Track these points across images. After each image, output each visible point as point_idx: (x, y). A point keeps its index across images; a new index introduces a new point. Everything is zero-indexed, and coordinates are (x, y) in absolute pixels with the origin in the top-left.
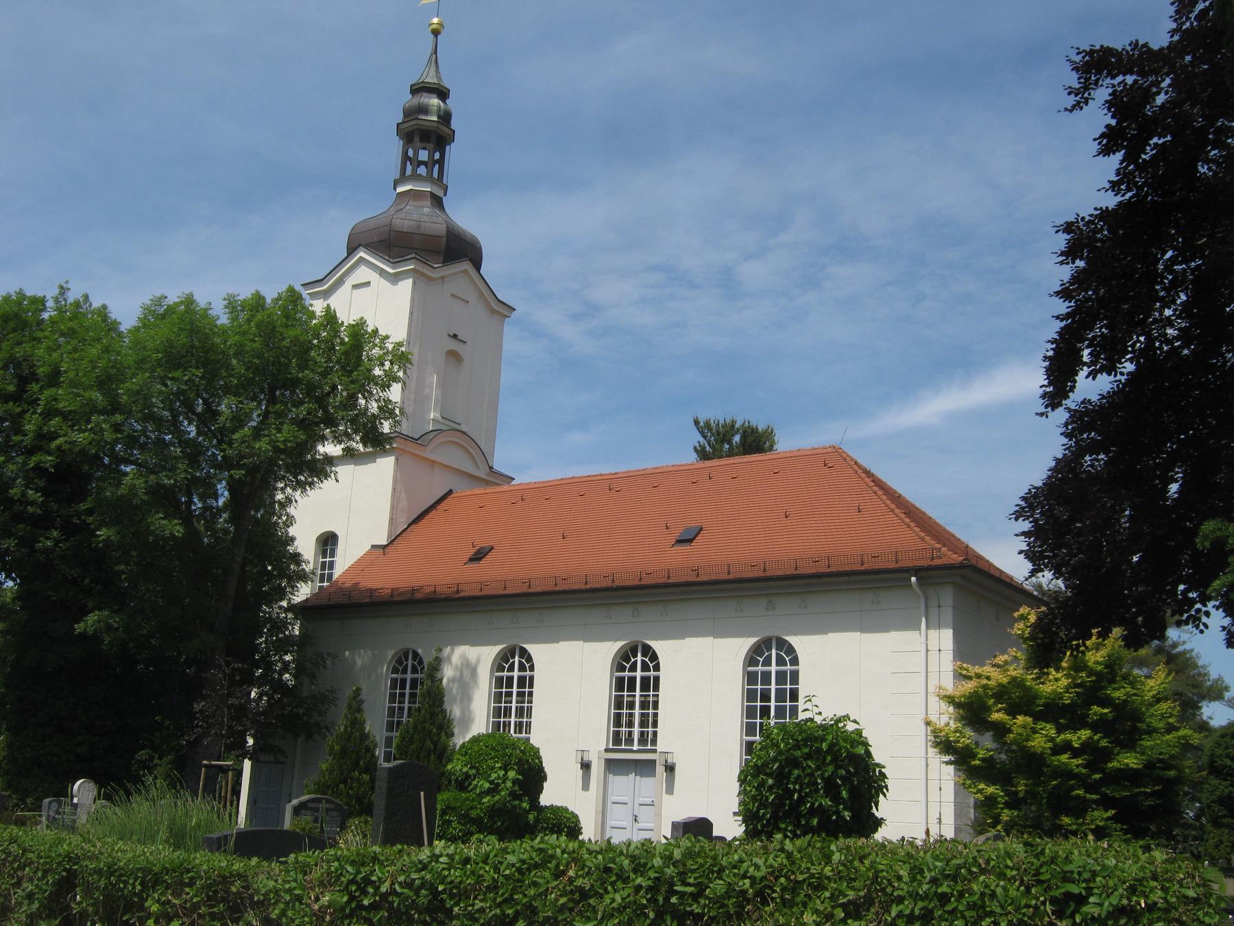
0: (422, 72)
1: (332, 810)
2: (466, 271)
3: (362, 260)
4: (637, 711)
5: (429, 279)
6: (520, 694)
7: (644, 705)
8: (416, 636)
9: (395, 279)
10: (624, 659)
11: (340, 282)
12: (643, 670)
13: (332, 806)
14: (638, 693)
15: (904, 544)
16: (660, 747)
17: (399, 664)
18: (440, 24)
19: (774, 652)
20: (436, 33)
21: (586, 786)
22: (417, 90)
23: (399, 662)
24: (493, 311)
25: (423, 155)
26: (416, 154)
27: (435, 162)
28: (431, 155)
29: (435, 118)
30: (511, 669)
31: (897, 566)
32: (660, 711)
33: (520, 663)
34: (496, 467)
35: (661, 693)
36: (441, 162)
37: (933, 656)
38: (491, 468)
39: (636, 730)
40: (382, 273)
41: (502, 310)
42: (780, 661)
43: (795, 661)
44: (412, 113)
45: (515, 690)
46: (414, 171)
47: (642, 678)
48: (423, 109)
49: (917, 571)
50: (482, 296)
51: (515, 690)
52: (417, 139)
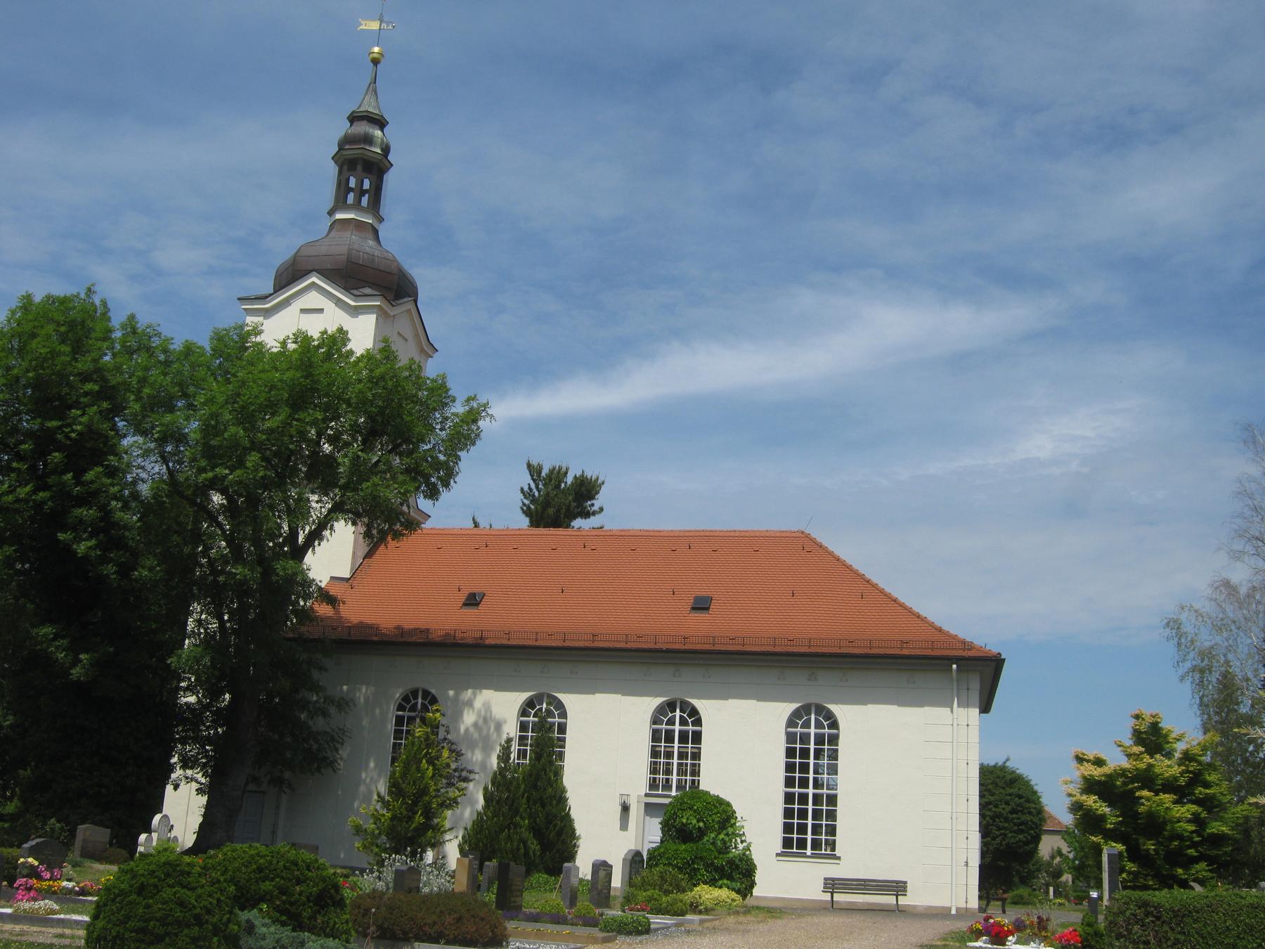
3: (314, 284)
4: (675, 761)
8: (425, 675)
9: (355, 312)
11: (286, 303)
12: (681, 724)
14: (676, 744)
17: (407, 701)
19: (813, 717)
21: (624, 825)
22: (353, 118)
40: (338, 302)
43: (698, 722)
44: (346, 141)
48: (368, 140)
49: (957, 660)
52: (359, 168)
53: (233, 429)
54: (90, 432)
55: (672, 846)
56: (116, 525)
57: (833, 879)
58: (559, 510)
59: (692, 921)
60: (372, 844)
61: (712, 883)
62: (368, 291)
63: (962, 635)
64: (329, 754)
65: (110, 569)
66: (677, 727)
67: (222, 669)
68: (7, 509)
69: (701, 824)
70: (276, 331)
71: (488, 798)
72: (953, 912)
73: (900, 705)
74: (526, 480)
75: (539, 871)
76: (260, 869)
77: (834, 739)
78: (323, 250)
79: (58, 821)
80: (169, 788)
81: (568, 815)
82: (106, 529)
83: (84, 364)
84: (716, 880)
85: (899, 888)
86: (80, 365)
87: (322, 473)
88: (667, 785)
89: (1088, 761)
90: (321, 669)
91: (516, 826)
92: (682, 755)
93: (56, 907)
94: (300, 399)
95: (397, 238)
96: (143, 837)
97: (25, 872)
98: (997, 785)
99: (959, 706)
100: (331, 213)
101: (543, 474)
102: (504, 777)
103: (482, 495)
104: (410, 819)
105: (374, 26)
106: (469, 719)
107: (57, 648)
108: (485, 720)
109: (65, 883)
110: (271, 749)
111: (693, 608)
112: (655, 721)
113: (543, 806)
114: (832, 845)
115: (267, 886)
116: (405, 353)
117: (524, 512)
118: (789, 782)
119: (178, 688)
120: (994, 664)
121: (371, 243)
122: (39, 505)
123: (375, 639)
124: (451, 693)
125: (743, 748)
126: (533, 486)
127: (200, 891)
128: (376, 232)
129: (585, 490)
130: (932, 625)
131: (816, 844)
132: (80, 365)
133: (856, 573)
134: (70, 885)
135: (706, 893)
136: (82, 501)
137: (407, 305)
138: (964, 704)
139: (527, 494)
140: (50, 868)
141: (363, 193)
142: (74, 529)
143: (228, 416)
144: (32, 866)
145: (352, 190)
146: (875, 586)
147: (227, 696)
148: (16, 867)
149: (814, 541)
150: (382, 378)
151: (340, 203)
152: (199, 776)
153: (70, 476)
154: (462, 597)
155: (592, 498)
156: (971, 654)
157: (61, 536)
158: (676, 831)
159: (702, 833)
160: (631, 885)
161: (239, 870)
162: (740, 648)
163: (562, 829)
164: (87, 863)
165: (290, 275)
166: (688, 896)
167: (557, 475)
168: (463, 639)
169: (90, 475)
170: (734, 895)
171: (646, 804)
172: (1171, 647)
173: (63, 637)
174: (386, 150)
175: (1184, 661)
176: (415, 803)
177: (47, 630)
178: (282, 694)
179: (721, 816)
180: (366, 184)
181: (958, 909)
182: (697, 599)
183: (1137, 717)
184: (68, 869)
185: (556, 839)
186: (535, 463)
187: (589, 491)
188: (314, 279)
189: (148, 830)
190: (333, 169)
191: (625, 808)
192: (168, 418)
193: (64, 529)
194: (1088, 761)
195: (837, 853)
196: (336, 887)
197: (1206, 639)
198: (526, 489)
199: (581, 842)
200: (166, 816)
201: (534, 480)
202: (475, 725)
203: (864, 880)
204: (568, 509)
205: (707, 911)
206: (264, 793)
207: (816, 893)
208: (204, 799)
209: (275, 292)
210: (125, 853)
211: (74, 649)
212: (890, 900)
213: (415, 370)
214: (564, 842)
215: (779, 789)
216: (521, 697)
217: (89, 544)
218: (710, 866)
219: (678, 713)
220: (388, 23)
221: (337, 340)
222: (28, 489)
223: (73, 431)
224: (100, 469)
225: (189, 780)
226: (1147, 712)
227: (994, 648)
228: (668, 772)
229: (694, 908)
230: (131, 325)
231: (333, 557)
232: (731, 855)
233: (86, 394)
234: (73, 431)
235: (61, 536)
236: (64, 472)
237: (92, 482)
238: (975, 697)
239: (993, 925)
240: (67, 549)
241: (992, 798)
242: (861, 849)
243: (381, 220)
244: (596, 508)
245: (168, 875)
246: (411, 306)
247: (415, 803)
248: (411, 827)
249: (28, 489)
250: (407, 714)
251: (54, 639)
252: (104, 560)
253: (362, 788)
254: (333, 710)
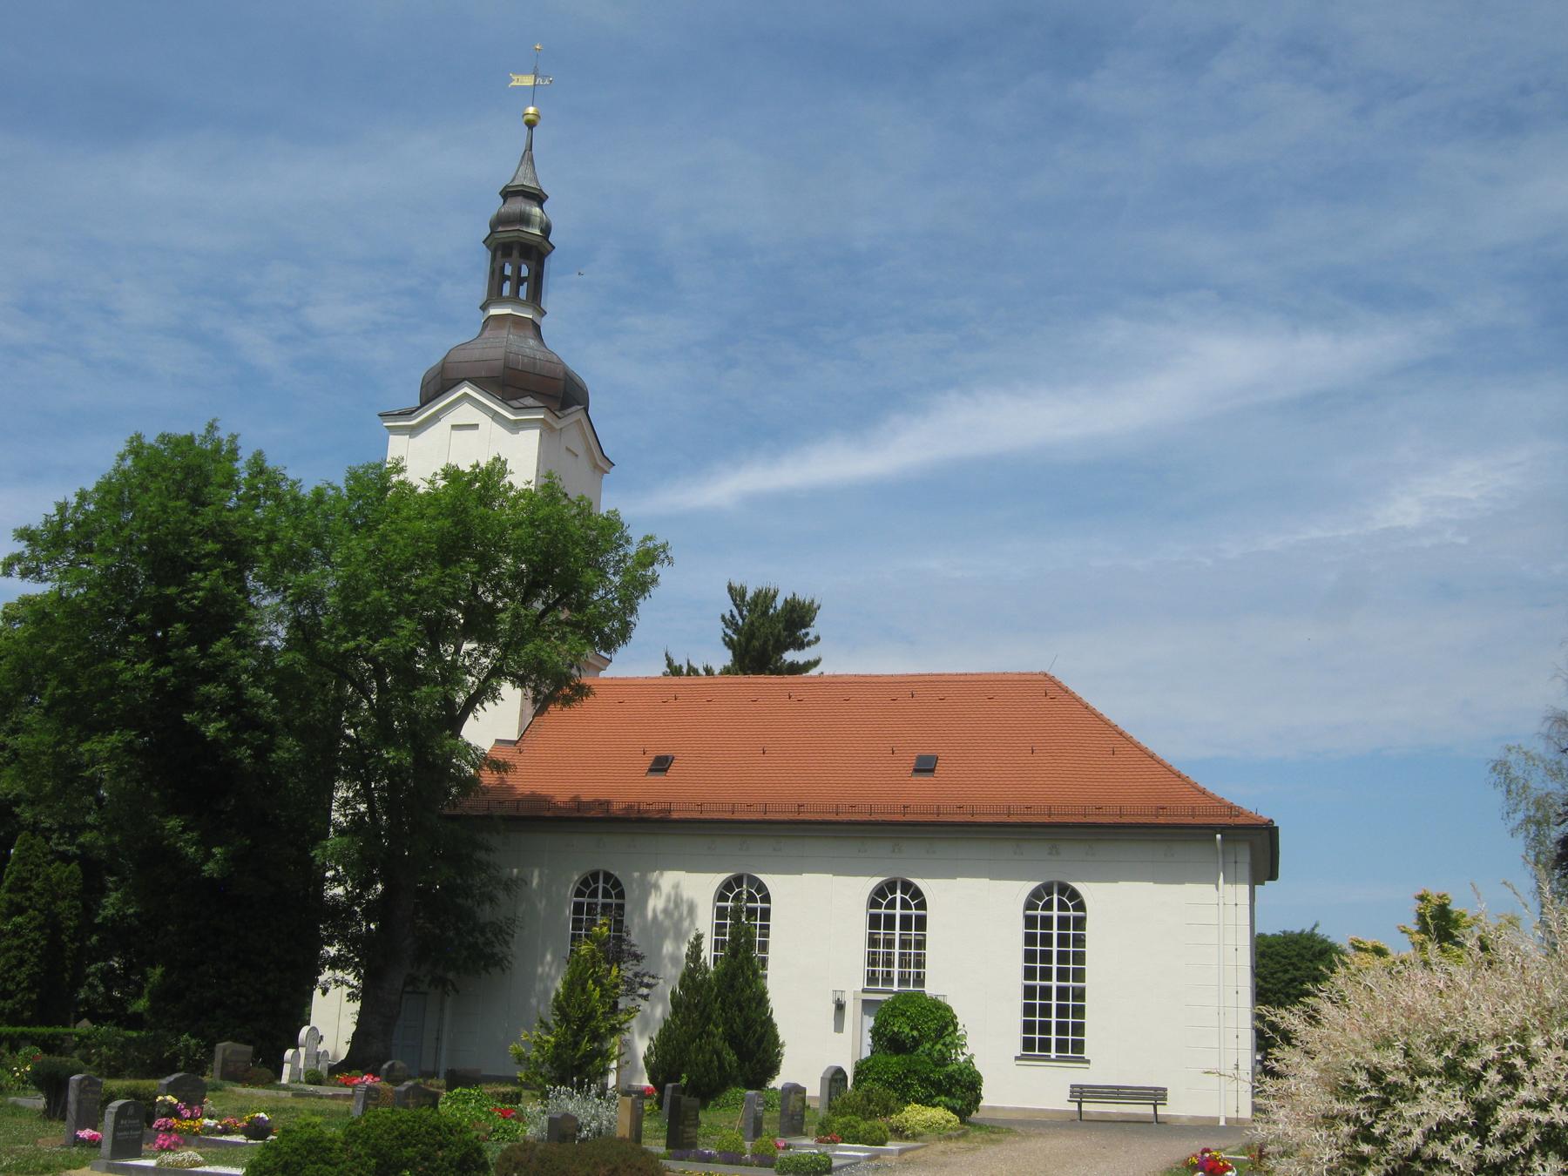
0: (507, 171)
3: (466, 396)
4: (897, 950)
9: (515, 427)
10: (879, 896)
11: (435, 418)
14: (897, 931)
17: (587, 885)
18: (537, 115)
19: (1055, 897)
20: (531, 125)
21: (839, 1027)
22: (507, 194)
29: (538, 232)
35: (928, 932)
39: (896, 970)
40: (496, 416)
42: (905, 905)
43: (922, 905)
44: (499, 221)
48: (525, 219)
52: (515, 253)
53: (375, 593)
54: (214, 596)
55: (882, 1058)
56: (249, 703)
57: (1081, 1087)
58: (765, 642)
59: (890, 1152)
60: (535, 1074)
61: (927, 1101)
62: (529, 401)
63: (1229, 799)
64: (496, 950)
65: (244, 753)
66: (898, 912)
67: (371, 853)
68: (125, 688)
69: (915, 1033)
70: (427, 456)
71: (676, 1003)
72: (1222, 1123)
73: (1156, 882)
74: (727, 607)
75: (737, 1085)
76: (402, 1136)
77: (1080, 923)
78: (476, 354)
79: (192, 1036)
80: (317, 993)
81: (770, 1019)
82: (237, 708)
83: (207, 516)
84: (931, 1097)
85: (1157, 1095)
86: (199, 520)
87: (480, 624)
88: (888, 979)
89: (1366, 950)
90: (488, 849)
91: (710, 1034)
92: (905, 944)
93: (200, 1158)
94: (451, 550)
95: (567, 330)
96: (289, 1053)
97: (164, 1110)
98: (1303, 957)
99: (1225, 882)
100: (484, 308)
101: (747, 598)
102: (693, 979)
103: (675, 627)
104: (576, 1044)
105: (528, 81)
106: (656, 903)
107: (186, 841)
108: (677, 905)
109: (206, 1121)
110: (432, 944)
111: (916, 771)
112: (873, 903)
113: (741, 1010)
114: (1079, 1046)
115: (409, 1152)
116: (575, 484)
117: (726, 644)
118: (1029, 973)
119: (325, 879)
120: (1266, 833)
121: (532, 342)
122: (161, 682)
123: (549, 814)
124: (636, 874)
125: (974, 934)
126: (736, 612)
127: (341, 1167)
128: (537, 328)
129: (797, 618)
130: (1194, 786)
131: (1062, 1046)
132: (199, 520)
133: (1106, 722)
134: (212, 1123)
135: (916, 1114)
136: (208, 677)
137: (575, 413)
138: (1232, 879)
139: (729, 622)
140: (189, 1105)
141: (521, 281)
142: (201, 708)
143: (368, 575)
144: (171, 1104)
145: (508, 278)
146: (1129, 739)
147: (379, 886)
148: (154, 1104)
149: (1058, 685)
150: (546, 520)
151: (495, 296)
152: (351, 978)
153: (194, 648)
154: (648, 762)
155: (807, 625)
156: (1240, 821)
157: (187, 717)
158: (886, 1040)
159: (917, 1043)
160: (830, 1108)
161: (381, 1137)
162: (969, 818)
163: (763, 1036)
164: (228, 1086)
165: (438, 385)
166: (895, 1119)
167: (764, 599)
168: (647, 811)
169: (217, 647)
170: (950, 1115)
171: (864, 1001)
172: (1498, 796)
173: (192, 830)
174: (546, 230)
175: (1515, 811)
176: (581, 1028)
177: (173, 823)
178: (445, 889)
179: (940, 1021)
180: (525, 272)
181: (1227, 1120)
182: (920, 758)
183: (1422, 898)
184: (209, 1104)
185: (757, 1048)
186: (737, 585)
187: (802, 618)
188: (466, 389)
189: (295, 1044)
190: (484, 258)
191: (840, 1007)
192: (302, 578)
193: (190, 707)
194: (1366, 950)
195: (1086, 1055)
196: (479, 1151)
197: (1541, 784)
198: (728, 616)
199: (785, 1050)
200: (314, 1029)
201: (737, 606)
202: (665, 911)
203: (1118, 1088)
204: (777, 641)
205: (915, 1136)
206: (425, 994)
207: (1060, 1101)
208: (357, 1005)
209: (423, 404)
210: (269, 1073)
211: (205, 843)
212: (1148, 1110)
213: (585, 510)
214: (766, 1051)
215: (1017, 982)
216: (718, 879)
217: (219, 725)
218: (925, 1081)
219: (898, 895)
220: (544, 77)
221: (498, 468)
222: (147, 664)
223: (194, 598)
224: (227, 640)
225: (339, 983)
226: (1434, 891)
227: (1265, 814)
228: (889, 963)
229: (899, 1133)
230: (258, 468)
231: (495, 723)
232: (950, 1068)
233: (207, 555)
234: (194, 598)
235: (187, 717)
236: (187, 645)
237: (219, 654)
238: (1245, 869)
239: (1207, 1160)
240: (193, 733)
241: (1297, 974)
242: (1112, 1055)
243: (543, 313)
244: (811, 637)
245: (310, 1152)
246: (581, 416)
247: (581, 1028)
248: (577, 1063)
249: (147, 664)
250: (585, 900)
251: (182, 832)
252: (237, 742)
253: (539, 987)
254: (501, 895)
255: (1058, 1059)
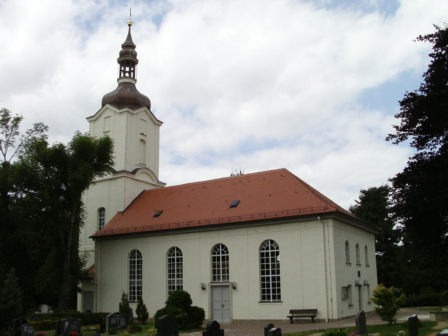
1: (122, 317)
2: (145, 110)
5: (132, 114)
6: (178, 264)
7: (223, 266)
13: (122, 315)
15: (319, 208)
16: (231, 280)
23: (132, 254)
24: (155, 124)
25: (127, 69)
26: (125, 69)
27: (132, 71)
28: (130, 69)
30: (174, 255)
31: (312, 213)
32: (230, 268)
33: (177, 253)
34: (160, 180)
35: (229, 261)
36: (134, 71)
37: (327, 243)
38: (158, 181)
39: (221, 275)
41: (159, 123)
45: (176, 263)
46: (124, 75)
47: (222, 257)
50: (151, 119)
51: (176, 263)
114: (279, 297)
131: (274, 297)
255: (273, 302)
